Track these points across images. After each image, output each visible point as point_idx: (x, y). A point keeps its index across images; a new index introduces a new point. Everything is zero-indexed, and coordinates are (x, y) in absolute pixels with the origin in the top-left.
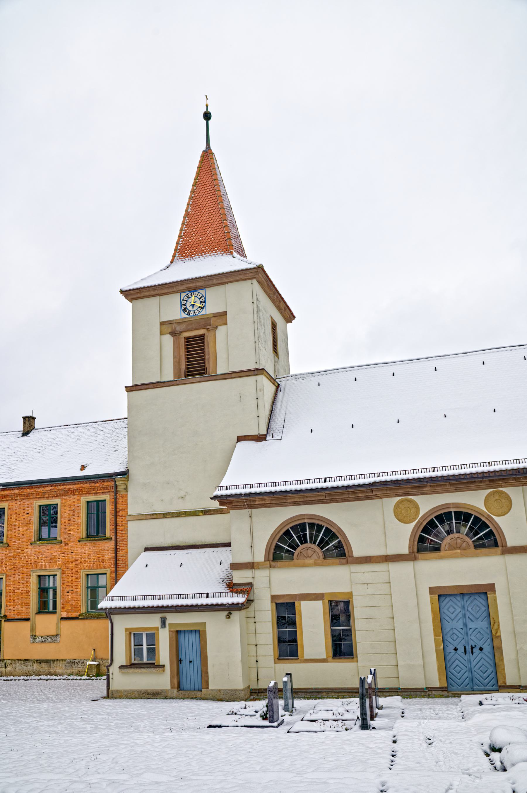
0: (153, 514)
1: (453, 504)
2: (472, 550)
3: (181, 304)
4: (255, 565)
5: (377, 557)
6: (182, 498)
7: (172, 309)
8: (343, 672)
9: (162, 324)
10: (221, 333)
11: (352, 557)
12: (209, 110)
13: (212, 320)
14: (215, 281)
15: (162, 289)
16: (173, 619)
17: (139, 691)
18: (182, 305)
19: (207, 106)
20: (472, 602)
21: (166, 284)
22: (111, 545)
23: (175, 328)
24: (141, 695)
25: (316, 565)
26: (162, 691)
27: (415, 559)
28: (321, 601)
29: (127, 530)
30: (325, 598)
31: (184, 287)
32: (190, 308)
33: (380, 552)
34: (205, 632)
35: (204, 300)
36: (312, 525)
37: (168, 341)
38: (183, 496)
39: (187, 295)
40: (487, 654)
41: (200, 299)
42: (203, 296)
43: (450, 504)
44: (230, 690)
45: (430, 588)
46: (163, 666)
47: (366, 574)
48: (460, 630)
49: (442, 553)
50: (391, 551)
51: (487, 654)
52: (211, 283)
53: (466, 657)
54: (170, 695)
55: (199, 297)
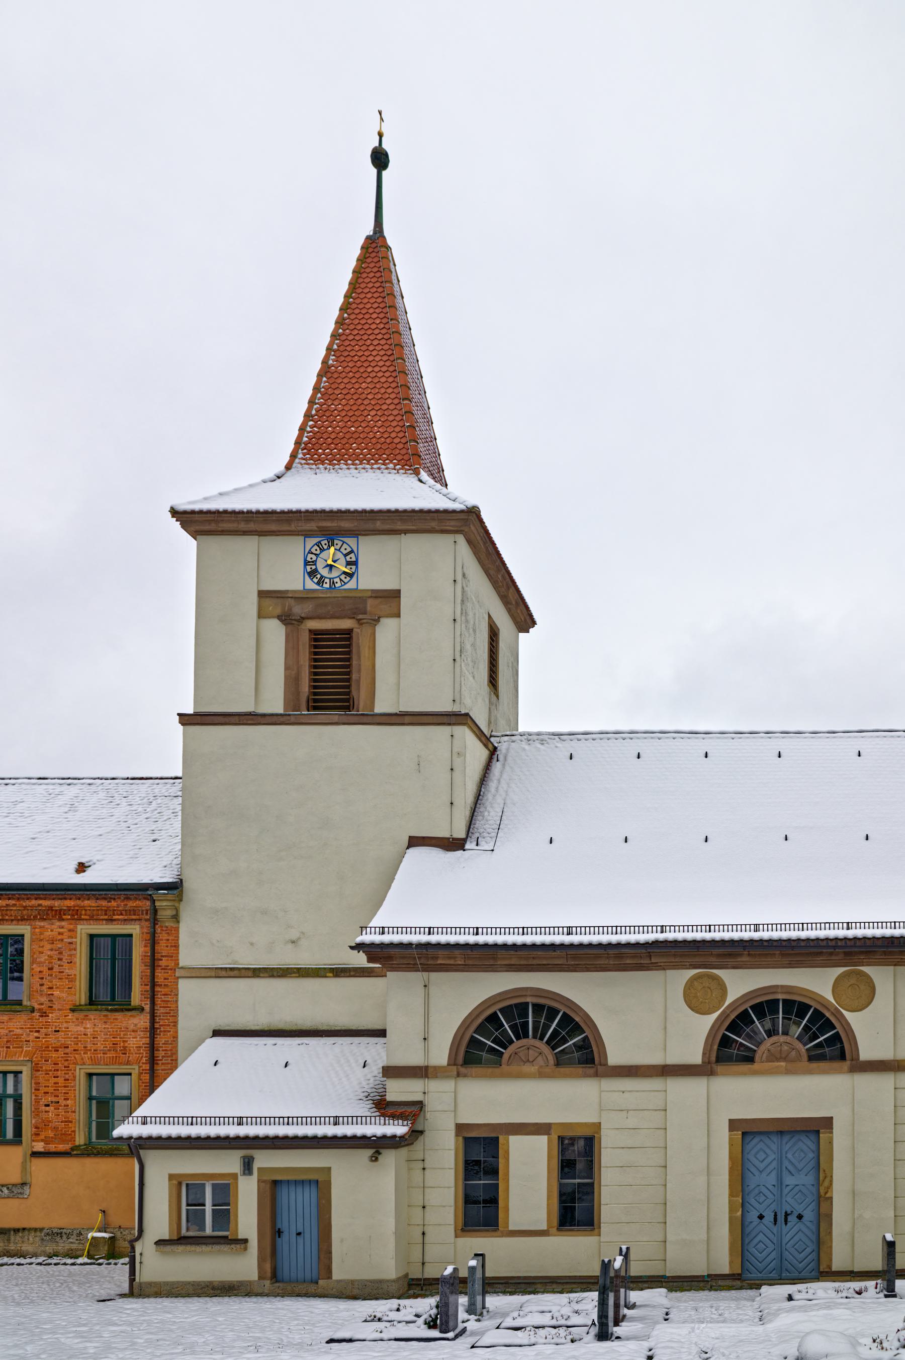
0: (231, 969)
1: (782, 986)
3: (305, 560)
4: (430, 1070)
6: (293, 942)
7: (285, 566)
8: (576, 1252)
9: (262, 594)
10: (386, 633)
11: (606, 1064)
13: (370, 602)
16: (264, 1160)
17: (194, 1284)
18: (306, 563)
19: (381, 135)
22: (142, 1021)
23: (290, 609)
29: (177, 995)
30: (552, 1131)
32: (325, 572)
33: (656, 1059)
35: (354, 559)
37: (275, 633)
38: (294, 938)
39: (318, 544)
40: (809, 1224)
41: (345, 555)
42: (352, 552)
43: (777, 986)
44: (372, 1281)
46: (245, 1241)
47: (626, 1095)
48: (771, 1187)
49: (756, 1066)
51: (809, 1224)
53: (775, 1229)
54: (256, 1289)
55: (345, 552)
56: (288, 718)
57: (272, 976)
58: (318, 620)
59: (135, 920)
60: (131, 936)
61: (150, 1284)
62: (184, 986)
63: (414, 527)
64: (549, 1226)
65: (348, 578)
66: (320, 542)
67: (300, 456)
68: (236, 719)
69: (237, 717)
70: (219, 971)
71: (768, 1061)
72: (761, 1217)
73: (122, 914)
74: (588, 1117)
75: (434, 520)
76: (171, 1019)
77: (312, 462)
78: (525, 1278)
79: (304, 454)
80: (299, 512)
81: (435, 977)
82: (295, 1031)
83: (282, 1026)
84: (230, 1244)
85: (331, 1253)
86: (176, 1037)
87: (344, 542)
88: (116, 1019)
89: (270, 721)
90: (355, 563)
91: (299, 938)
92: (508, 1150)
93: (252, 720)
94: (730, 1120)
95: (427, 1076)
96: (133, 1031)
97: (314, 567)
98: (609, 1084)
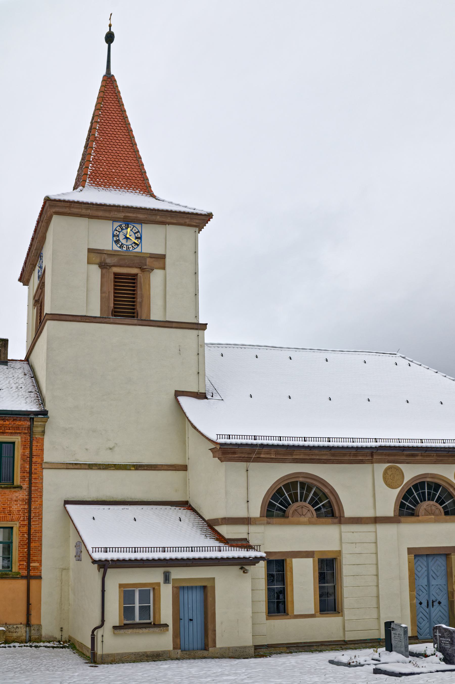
0: (76, 464)
1: (431, 474)
2: (443, 516)
3: (113, 234)
4: (252, 520)
5: (367, 518)
6: (111, 449)
7: (102, 236)
8: (327, 627)
9: (90, 251)
10: (156, 277)
11: (344, 517)
12: (112, 30)
13: (148, 260)
14: (158, 217)
15: (97, 210)
16: (178, 574)
17: (135, 654)
18: (114, 236)
19: (110, 26)
20: (435, 562)
21: (105, 205)
22: (22, 495)
23: (105, 260)
24: (139, 658)
25: (310, 523)
26: (164, 652)
27: (399, 522)
28: (312, 559)
29: (42, 479)
30: (315, 556)
31: (121, 215)
32: (124, 241)
33: (370, 514)
34: (213, 588)
35: (139, 236)
36: (303, 485)
37: (96, 272)
38: (111, 447)
39: (120, 226)
40: (444, 607)
41: (135, 233)
42: (138, 232)
43: (428, 474)
44: (239, 647)
45: (408, 548)
46: (166, 625)
47: (355, 533)
48: (424, 586)
49: (420, 518)
50: (380, 514)
51: (444, 607)
52: (153, 218)
53: (427, 610)
54: (173, 655)
55: (135, 232)
56: (109, 320)
57: (100, 469)
58: (119, 268)
59: (18, 433)
60: (14, 443)
61: (108, 655)
62: (46, 473)
63: (175, 221)
64: (316, 611)
65: (136, 246)
66: (121, 225)
67: (88, 181)
68: (79, 319)
69: (80, 317)
70: (69, 465)
71: (425, 515)
72: (421, 603)
73: (9, 429)
74: (334, 547)
75: (187, 218)
76: (39, 494)
77: (94, 185)
78: (305, 643)
79: (90, 181)
80: (119, 206)
81: (252, 465)
82: (112, 502)
83: (104, 499)
84: (160, 627)
85: (215, 631)
86: (41, 505)
87: (134, 226)
88: (5, 493)
89: (98, 321)
90: (140, 238)
91: (114, 447)
92: (292, 567)
93: (89, 319)
94: (408, 548)
95: (248, 524)
96: (15, 501)
97: (118, 238)
98: (345, 528)
